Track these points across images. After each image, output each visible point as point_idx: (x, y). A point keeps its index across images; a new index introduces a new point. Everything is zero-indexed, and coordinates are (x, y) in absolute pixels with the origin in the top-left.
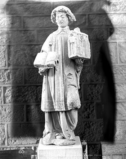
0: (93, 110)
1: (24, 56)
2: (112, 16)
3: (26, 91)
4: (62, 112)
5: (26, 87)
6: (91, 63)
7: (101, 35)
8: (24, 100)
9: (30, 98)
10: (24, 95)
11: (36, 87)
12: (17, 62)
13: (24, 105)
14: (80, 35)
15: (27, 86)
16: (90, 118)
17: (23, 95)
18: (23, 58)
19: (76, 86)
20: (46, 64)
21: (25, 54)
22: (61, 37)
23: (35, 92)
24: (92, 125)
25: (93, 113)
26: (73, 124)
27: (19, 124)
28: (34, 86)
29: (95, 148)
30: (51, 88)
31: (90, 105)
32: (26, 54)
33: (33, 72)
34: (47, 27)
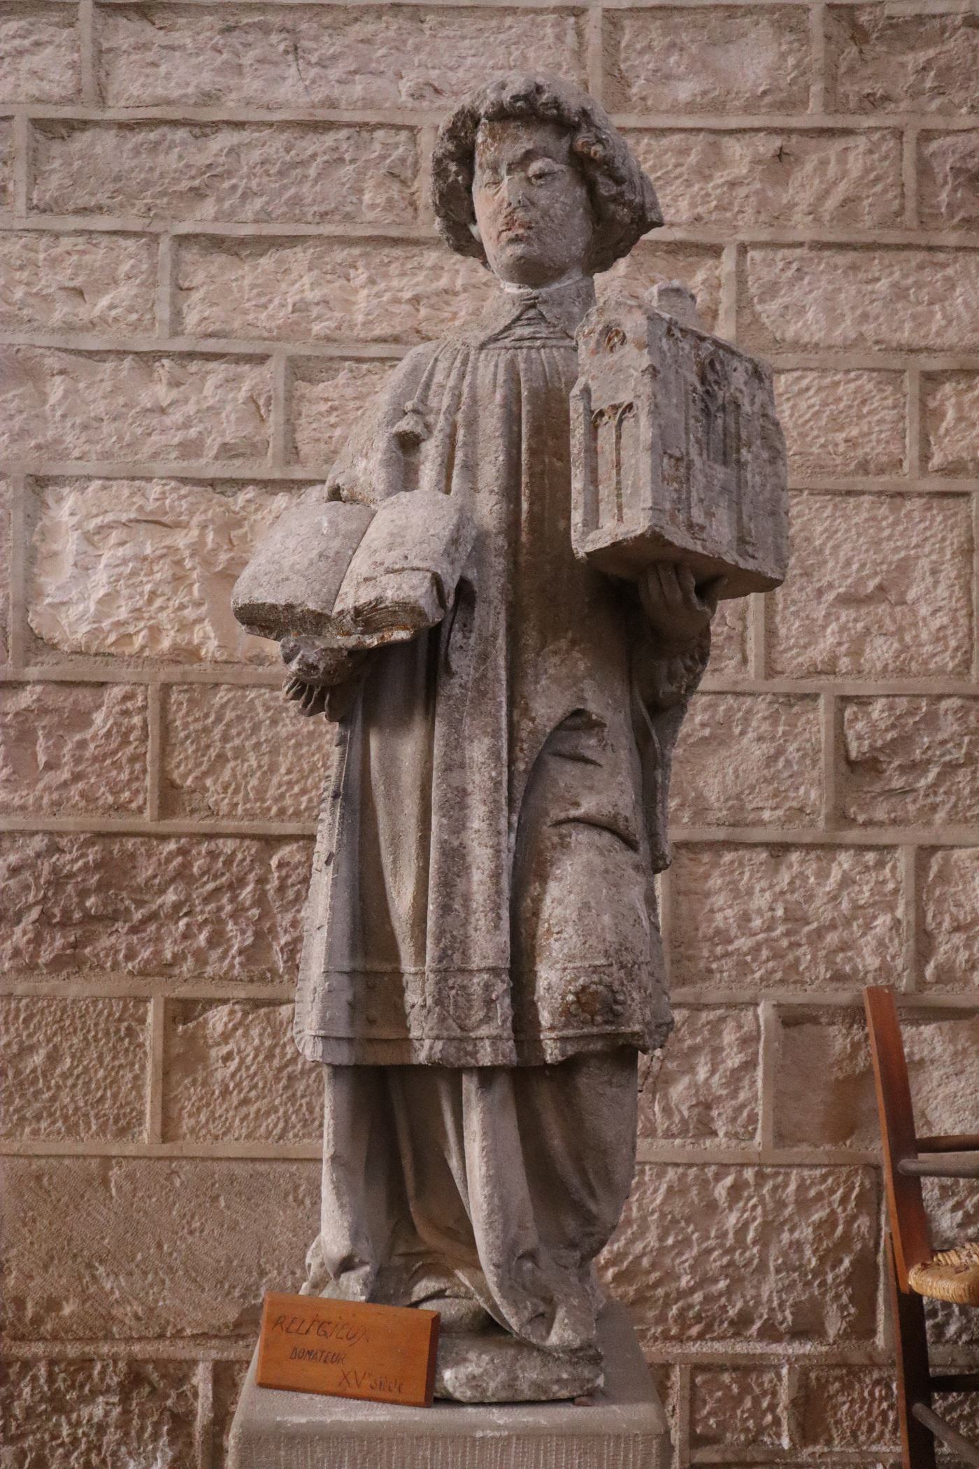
0: (749, 1065)
1: (163, 571)
2: (944, 266)
3: (172, 880)
4: (487, 1076)
5: (172, 846)
6: (745, 661)
7: (841, 428)
8: (146, 954)
9: (202, 938)
10: (153, 917)
11: (254, 847)
12: (106, 624)
13: (142, 1001)
15: (178, 836)
16: (714, 1133)
17: (138, 916)
18: (153, 595)
19: (639, 835)
20: (351, 597)
21: (179, 563)
22: (512, 366)
23: (246, 893)
24: (736, 1191)
25: (743, 1096)
26: (592, 1194)
27: (94, 1163)
28: (242, 836)
29: (748, 1403)
30: (395, 840)
31: (722, 1019)
32: (188, 564)
33: (240, 718)
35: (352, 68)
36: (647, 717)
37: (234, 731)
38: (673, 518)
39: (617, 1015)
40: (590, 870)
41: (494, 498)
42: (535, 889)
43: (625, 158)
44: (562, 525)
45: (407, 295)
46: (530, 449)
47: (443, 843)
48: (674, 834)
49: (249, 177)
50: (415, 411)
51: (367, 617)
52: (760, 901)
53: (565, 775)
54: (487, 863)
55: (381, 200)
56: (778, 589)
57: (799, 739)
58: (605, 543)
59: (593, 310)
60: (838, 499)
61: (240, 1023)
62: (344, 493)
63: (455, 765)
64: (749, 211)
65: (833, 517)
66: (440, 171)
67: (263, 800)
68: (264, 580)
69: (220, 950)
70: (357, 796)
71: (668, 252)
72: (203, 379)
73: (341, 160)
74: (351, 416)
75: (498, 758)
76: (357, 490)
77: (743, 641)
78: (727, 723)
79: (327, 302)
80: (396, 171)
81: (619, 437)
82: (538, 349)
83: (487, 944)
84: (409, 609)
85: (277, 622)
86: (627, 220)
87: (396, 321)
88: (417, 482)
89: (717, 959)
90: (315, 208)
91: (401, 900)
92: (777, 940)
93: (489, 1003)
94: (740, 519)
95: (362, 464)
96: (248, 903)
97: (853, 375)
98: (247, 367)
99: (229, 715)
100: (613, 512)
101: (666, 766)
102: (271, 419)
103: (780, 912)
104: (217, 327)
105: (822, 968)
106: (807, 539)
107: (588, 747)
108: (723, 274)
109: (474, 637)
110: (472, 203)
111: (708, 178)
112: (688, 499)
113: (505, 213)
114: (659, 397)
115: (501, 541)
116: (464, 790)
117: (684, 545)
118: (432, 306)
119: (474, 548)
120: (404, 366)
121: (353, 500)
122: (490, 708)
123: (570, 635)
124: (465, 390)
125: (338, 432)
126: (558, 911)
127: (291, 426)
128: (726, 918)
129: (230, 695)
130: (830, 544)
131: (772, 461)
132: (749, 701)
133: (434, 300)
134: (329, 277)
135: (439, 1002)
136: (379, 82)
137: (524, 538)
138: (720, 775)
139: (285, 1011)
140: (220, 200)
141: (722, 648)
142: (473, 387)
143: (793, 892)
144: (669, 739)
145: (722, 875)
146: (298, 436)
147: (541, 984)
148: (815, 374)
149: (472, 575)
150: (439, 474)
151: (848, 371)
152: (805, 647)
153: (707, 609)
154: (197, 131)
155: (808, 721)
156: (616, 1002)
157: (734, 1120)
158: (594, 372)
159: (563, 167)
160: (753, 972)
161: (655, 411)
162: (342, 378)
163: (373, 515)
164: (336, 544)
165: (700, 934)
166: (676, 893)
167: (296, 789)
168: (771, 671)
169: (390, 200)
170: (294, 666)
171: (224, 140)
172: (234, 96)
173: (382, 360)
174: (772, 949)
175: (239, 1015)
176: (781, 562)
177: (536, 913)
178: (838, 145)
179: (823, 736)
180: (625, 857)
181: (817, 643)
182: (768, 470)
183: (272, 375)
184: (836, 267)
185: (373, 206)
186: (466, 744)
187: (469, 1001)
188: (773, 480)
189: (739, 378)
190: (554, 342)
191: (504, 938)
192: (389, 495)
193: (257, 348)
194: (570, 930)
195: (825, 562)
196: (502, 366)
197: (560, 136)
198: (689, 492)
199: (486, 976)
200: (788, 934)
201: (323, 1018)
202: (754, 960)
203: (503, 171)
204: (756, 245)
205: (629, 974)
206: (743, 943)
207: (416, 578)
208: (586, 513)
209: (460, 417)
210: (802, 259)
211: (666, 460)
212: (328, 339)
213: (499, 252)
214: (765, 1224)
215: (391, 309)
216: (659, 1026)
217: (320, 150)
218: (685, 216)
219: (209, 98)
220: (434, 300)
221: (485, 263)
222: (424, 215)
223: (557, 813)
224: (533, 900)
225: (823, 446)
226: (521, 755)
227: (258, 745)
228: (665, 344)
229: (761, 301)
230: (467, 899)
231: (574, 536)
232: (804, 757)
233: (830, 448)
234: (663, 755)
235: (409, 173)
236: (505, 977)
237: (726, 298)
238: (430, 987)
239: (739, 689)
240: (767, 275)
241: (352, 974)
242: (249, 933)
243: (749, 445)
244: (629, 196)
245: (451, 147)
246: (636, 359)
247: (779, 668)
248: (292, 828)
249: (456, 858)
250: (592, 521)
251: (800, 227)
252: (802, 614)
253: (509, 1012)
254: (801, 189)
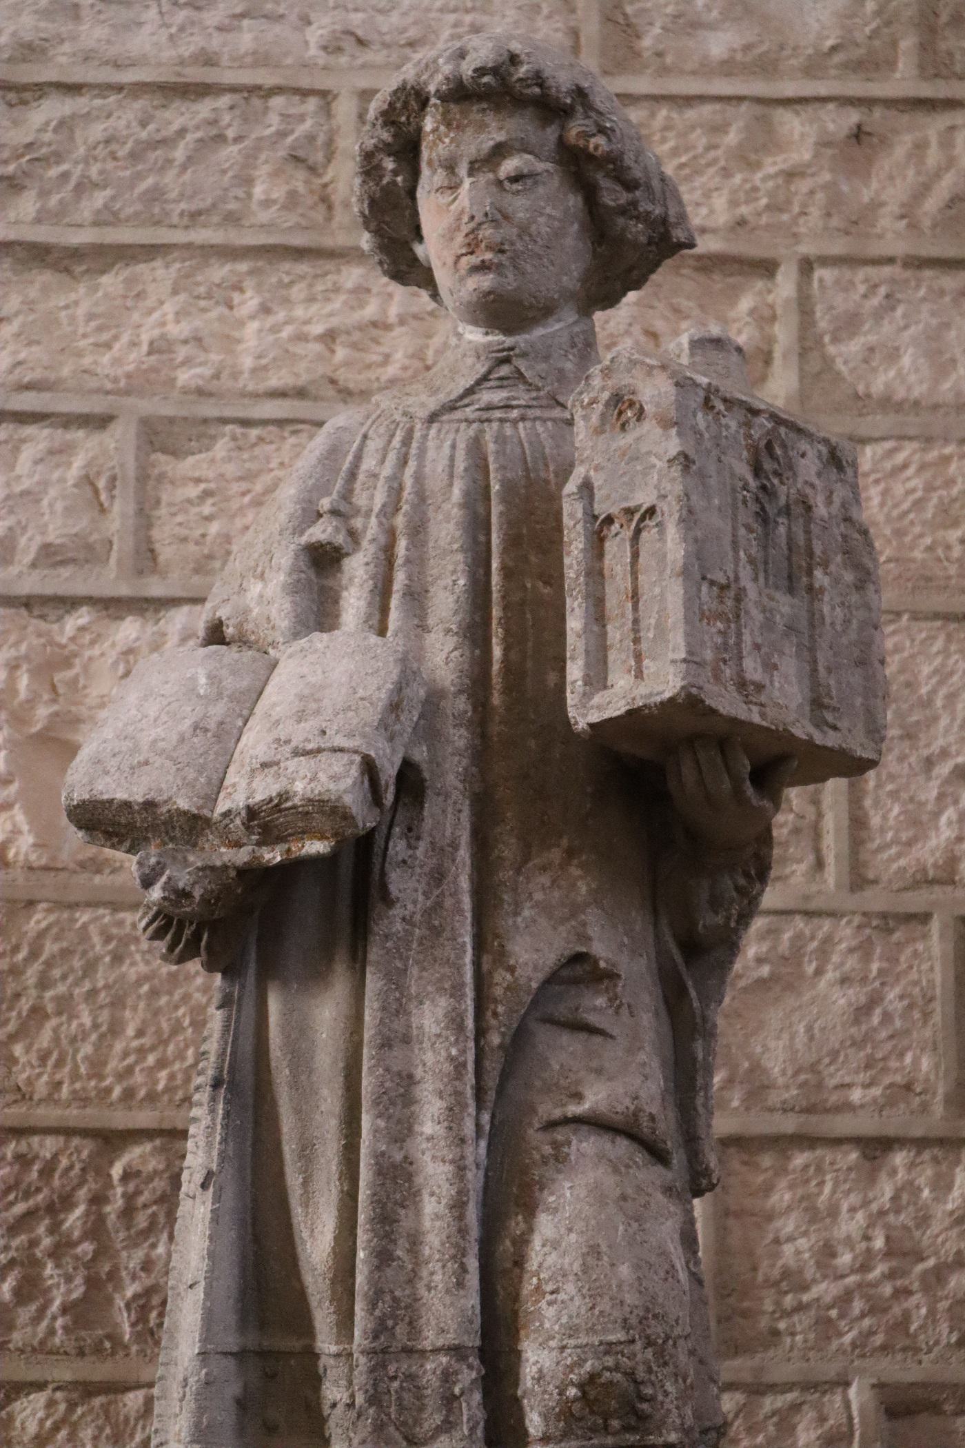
6: (820, 864)
11: (87, 1148)
14: (740, 414)
20: (242, 790)
22: (476, 447)
23: (74, 1219)
28: (68, 1132)
30: (307, 1152)
31: (796, 1407)
33: (66, 953)
34: (280, 394)
35: (238, 10)
36: (678, 958)
37: (56, 973)
38: (717, 677)
39: (642, 1417)
40: (599, 1196)
41: (451, 642)
42: (516, 1224)
43: (639, 153)
44: (552, 678)
45: (318, 329)
46: (504, 568)
47: (379, 1156)
48: (722, 1125)
49: (87, 163)
50: (335, 512)
51: (265, 821)
52: (850, 1225)
53: (561, 1052)
54: (446, 1186)
55: (279, 193)
56: (871, 774)
57: (903, 982)
58: (617, 709)
59: (595, 370)
60: (953, 626)
61: (64, 1421)
62: (229, 631)
63: (397, 1038)
64: (815, 212)
65: (945, 652)
66: (370, 167)
67: (101, 1077)
68: (112, 764)
69: (33, 1307)
70: (247, 1080)
71: (697, 269)
72: (16, 450)
73: (220, 138)
74: (235, 505)
75: (461, 1028)
76: (249, 626)
77: (816, 833)
78: (795, 956)
79: (198, 340)
80: (300, 153)
81: (635, 555)
82: (515, 422)
83: (446, 1309)
84: (325, 811)
85: (131, 826)
86: (643, 239)
87: (301, 366)
88: (338, 616)
89: (787, 1314)
90: (183, 206)
91: (316, 1242)
92: (875, 1285)
93: (450, 1401)
94: (815, 670)
95: (255, 588)
96: (76, 1234)
98: (81, 434)
99: (50, 948)
100: (630, 661)
101: (709, 1034)
102: (117, 508)
103: (879, 1243)
104: (37, 374)
105: (944, 1327)
106: (908, 684)
107: (595, 1009)
108: (779, 301)
109: (422, 846)
110: (415, 214)
111: (755, 166)
112: (738, 644)
113: (465, 229)
114: (694, 498)
115: (463, 704)
116: (410, 1076)
117: (733, 713)
118: (355, 346)
119: (421, 716)
120: (319, 442)
121: (242, 641)
122: (448, 952)
123: (565, 842)
124: (408, 482)
125: (214, 528)
127: (145, 517)
128: (798, 1252)
129: (52, 918)
130: (943, 692)
131: (860, 586)
132: (827, 925)
133: (356, 336)
134: (202, 303)
135: (374, 1399)
136: (277, 28)
137: (496, 699)
138: (786, 1036)
139: (133, 1401)
140: (44, 194)
141: (786, 844)
142: (419, 478)
143: (898, 1212)
144: (713, 996)
145: (791, 1187)
146: (155, 533)
147: (528, 1372)
148: (915, 445)
149: (420, 754)
150: (370, 604)
152: (909, 844)
153: (766, 804)
154: (12, 96)
155: (916, 954)
156: (643, 1399)
158: (598, 460)
159: (549, 166)
160: (840, 1335)
161: (689, 518)
162: (221, 448)
163: (274, 665)
164: (218, 710)
165: (760, 1278)
166: (723, 1215)
167: (151, 1059)
168: (858, 880)
169: (292, 195)
170: (156, 893)
171: (52, 109)
172: (67, 47)
173: (281, 423)
174: (868, 1298)
175: (62, 1407)
176: (875, 732)
177: (519, 1262)
178: (942, 121)
179: (938, 977)
180: (650, 1175)
181: (927, 837)
182: (854, 598)
183: (116, 446)
184: (942, 293)
185: (267, 203)
186: (412, 1007)
187: (420, 1398)
188: (861, 614)
189: (809, 466)
190: (538, 412)
191: (472, 1300)
192: (296, 635)
193: (96, 405)
194: (570, 1288)
195: (935, 719)
196: (461, 446)
197: (545, 121)
198: (739, 635)
199: (444, 1360)
200: (891, 1275)
201: (197, 1425)
202: (842, 1316)
203: (463, 170)
204: (825, 261)
205: (660, 1353)
206: (824, 1290)
207: (337, 764)
208: (587, 665)
209: (400, 521)
210: (892, 281)
211: (705, 588)
212: (201, 392)
213: (457, 283)
215: (292, 349)
216: (705, 1432)
217: (191, 124)
218: (722, 218)
219: (29, 51)
220: (356, 336)
221: (435, 295)
222: (340, 216)
223: (548, 1109)
224: (514, 1243)
225: (930, 549)
226: (493, 1022)
227: (93, 992)
228: (701, 420)
229: (835, 340)
230: (415, 1241)
231: (571, 699)
232: (911, 1007)
233: (940, 552)
234: (705, 1019)
235: (320, 156)
236: (474, 1360)
237: (784, 334)
238: (360, 1377)
240: (841, 302)
241: (240, 1356)
242: (79, 1280)
243: (825, 564)
244: (644, 206)
245: (386, 136)
246: (659, 444)
247: (871, 876)
248: (144, 1118)
249: (398, 1178)
250: (597, 679)
251: (889, 236)
252: (904, 796)
253: (480, 1415)
254: (888, 184)
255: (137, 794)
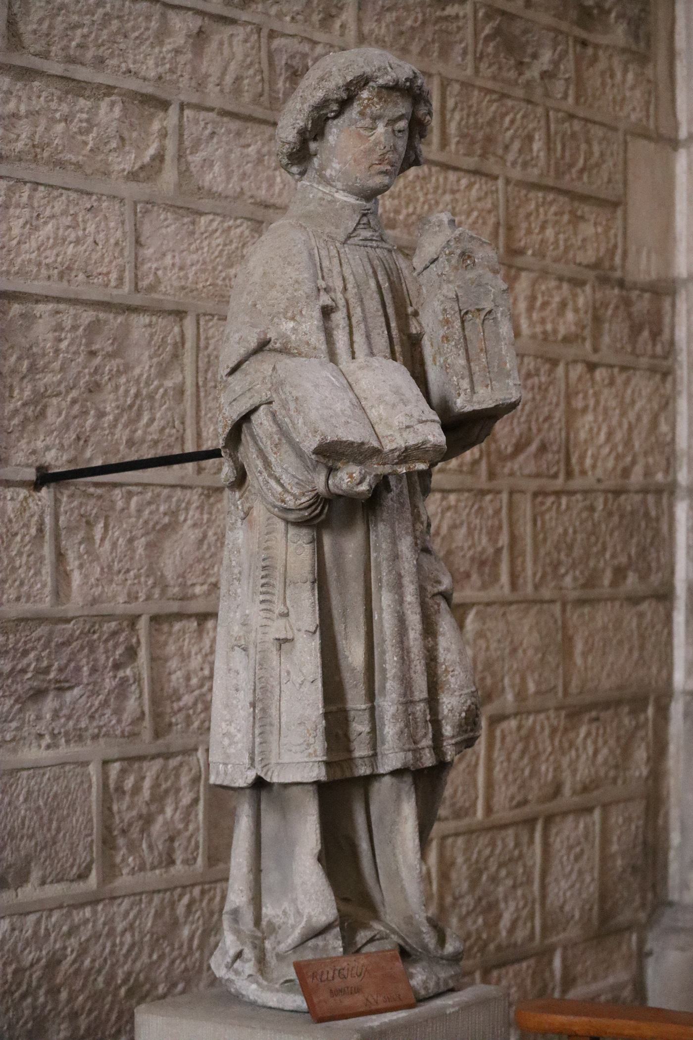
25: (191, 827)
64: (187, 76)
89: (175, 713)
97: (239, 222)
126: (449, 656)
151: (236, 219)
157: (186, 849)
194: (458, 669)
202: (194, 713)
204: (190, 105)
214: (204, 931)
225: (224, 279)
229: (191, 153)
239: (185, 483)
255: (358, 440)
